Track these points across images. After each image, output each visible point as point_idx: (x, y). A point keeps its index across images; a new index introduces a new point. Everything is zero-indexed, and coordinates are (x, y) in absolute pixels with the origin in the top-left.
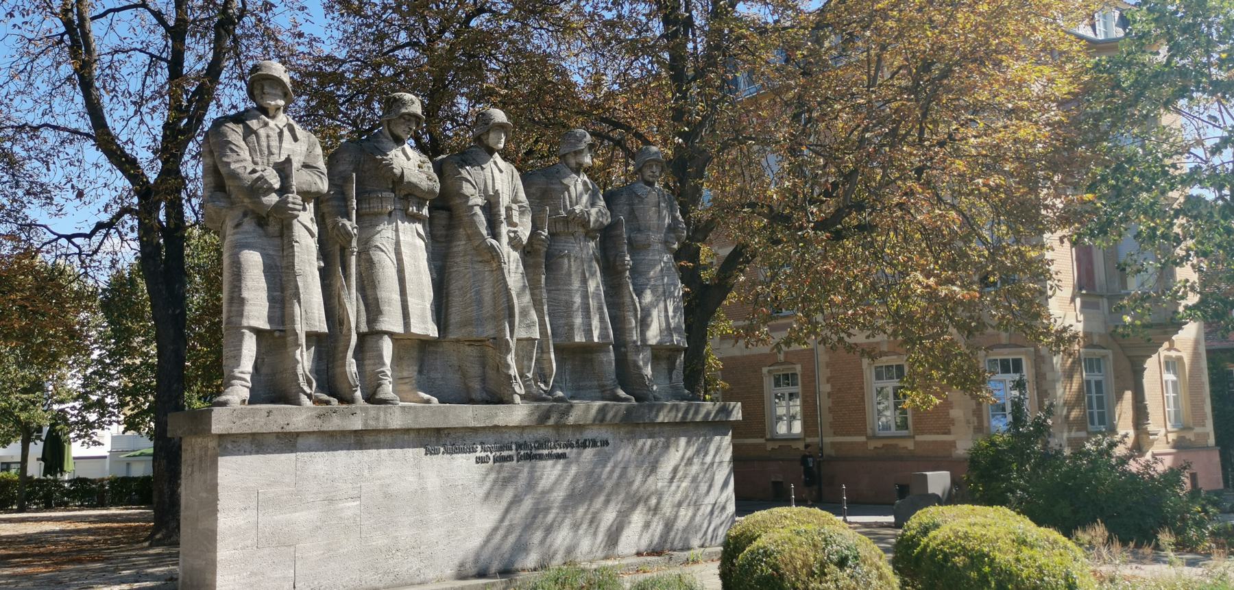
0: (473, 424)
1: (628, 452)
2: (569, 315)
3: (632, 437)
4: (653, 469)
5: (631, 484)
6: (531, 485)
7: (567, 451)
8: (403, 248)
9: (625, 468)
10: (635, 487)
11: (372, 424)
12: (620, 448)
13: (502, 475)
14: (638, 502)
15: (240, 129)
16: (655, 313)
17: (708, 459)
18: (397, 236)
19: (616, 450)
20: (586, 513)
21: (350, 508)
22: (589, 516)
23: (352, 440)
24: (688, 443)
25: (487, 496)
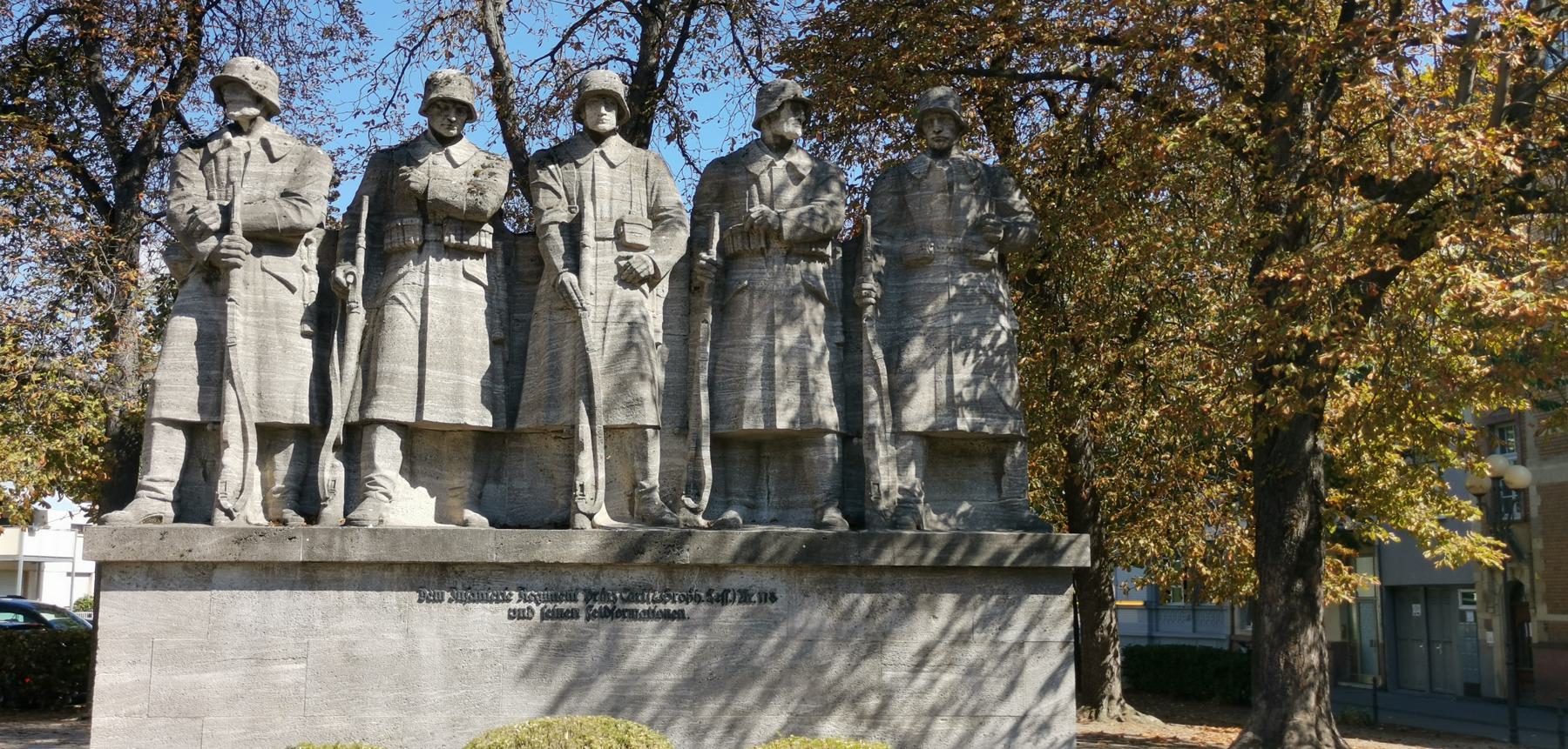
0: (494, 557)
1: (817, 615)
2: (741, 386)
3: (830, 588)
4: (875, 645)
5: (821, 670)
6: (611, 659)
7: (688, 608)
8: (448, 300)
9: (810, 643)
10: (832, 674)
11: (321, 554)
12: (801, 607)
13: (554, 641)
14: (839, 700)
15: (197, 157)
16: (926, 379)
17: (1011, 636)
18: (427, 280)
19: (792, 609)
20: (722, 711)
21: (290, 672)
22: (727, 717)
23: (298, 575)
24: (961, 605)
25: (526, 673)
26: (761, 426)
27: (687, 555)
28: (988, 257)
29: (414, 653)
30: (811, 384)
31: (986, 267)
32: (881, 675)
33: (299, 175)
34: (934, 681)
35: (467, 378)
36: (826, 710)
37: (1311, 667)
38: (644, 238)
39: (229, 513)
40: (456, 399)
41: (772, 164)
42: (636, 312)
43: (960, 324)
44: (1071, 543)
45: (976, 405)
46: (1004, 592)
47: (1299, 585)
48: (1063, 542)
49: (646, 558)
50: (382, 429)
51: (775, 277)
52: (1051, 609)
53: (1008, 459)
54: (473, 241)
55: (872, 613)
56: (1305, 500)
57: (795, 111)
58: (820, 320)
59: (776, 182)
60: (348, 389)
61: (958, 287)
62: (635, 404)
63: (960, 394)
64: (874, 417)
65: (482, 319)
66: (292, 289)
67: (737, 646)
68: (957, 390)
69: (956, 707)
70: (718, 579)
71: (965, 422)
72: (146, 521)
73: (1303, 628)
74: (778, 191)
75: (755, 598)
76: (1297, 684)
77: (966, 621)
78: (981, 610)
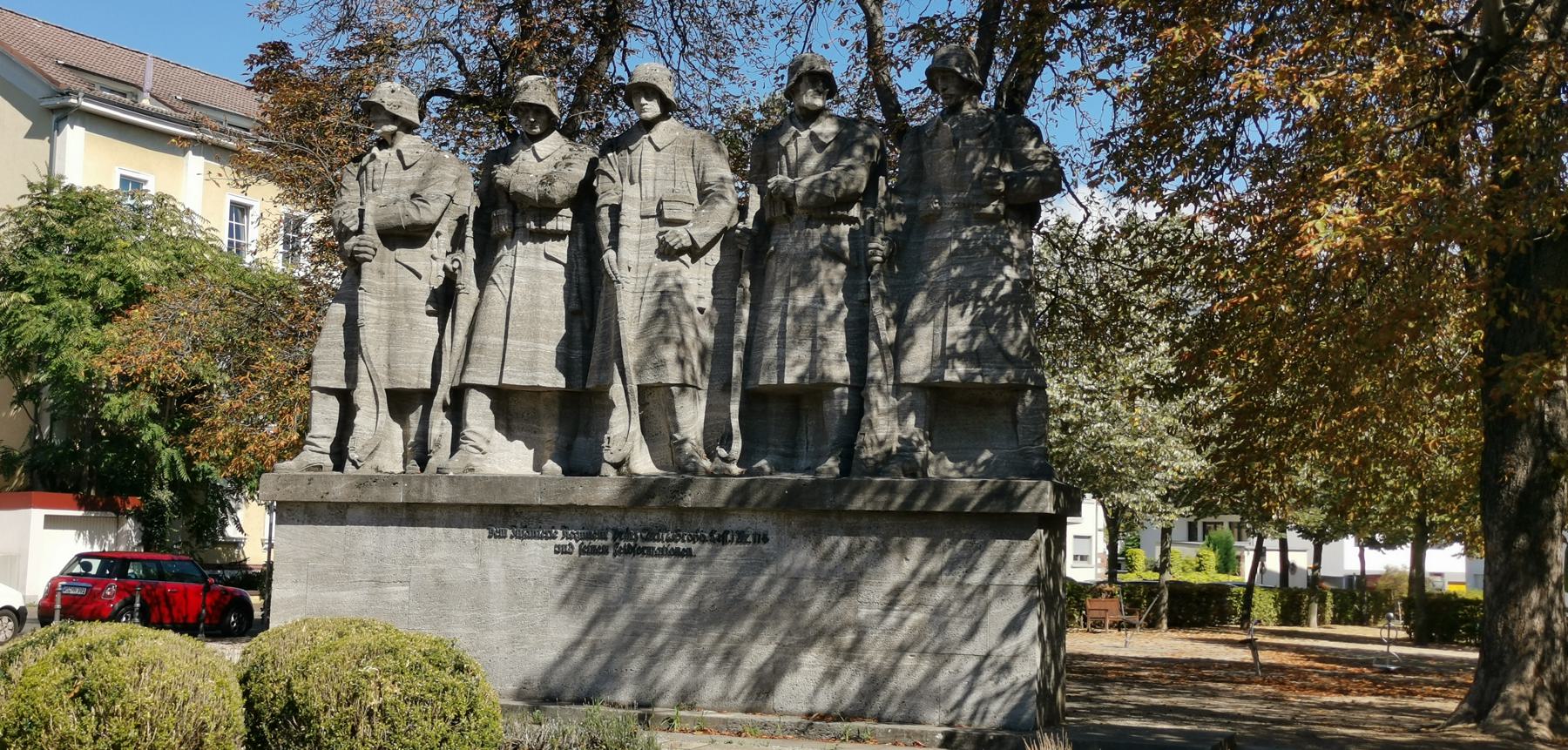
0: (539, 501)
3: (814, 533)
4: (850, 586)
5: (804, 606)
7: (694, 546)
8: (536, 273)
9: (795, 580)
10: (814, 609)
11: (415, 497)
14: (821, 633)
17: (976, 578)
19: (782, 549)
23: (404, 514)
24: (930, 549)
25: (565, 600)
26: (775, 381)
27: (689, 500)
28: (990, 209)
29: (485, 580)
30: (819, 342)
31: (993, 219)
32: (857, 612)
33: (425, 180)
34: (903, 619)
35: (542, 346)
36: (808, 643)
37: (1533, 634)
38: (685, 213)
39: (354, 463)
40: (532, 365)
41: (796, 135)
42: (669, 282)
43: (959, 277)
44: (1029, 489)
45: (970, 357)
46: (972, 537)
47: (1522, 541)
48: (1022, 489)
49: (654, 503)
50: (473, 392)
51: (796, 241)
52: (1016, 554)
53: (1020, 407)
54: (551, 225)
55: (849, 556)
56: (1525, 445)
57: (813, 84)
58: (837, 280)
59: (801, 151)
60: (455, 359)
61: (960, 241)
62: (660, 365)
63: (953, 346)
64: (876, 371)
65: (560, 293)
66: (419, 276)
67: (733, 582)
68: (949, 342)
69: (924, 644)
70: (720, 521)
71: (955, 373)
72: (308, 469)
73: (1526, 589)
74: (802, 160)
75: (750, 539)
76: (1515, 651)
77: (934, 564)
78: (947, 556)
